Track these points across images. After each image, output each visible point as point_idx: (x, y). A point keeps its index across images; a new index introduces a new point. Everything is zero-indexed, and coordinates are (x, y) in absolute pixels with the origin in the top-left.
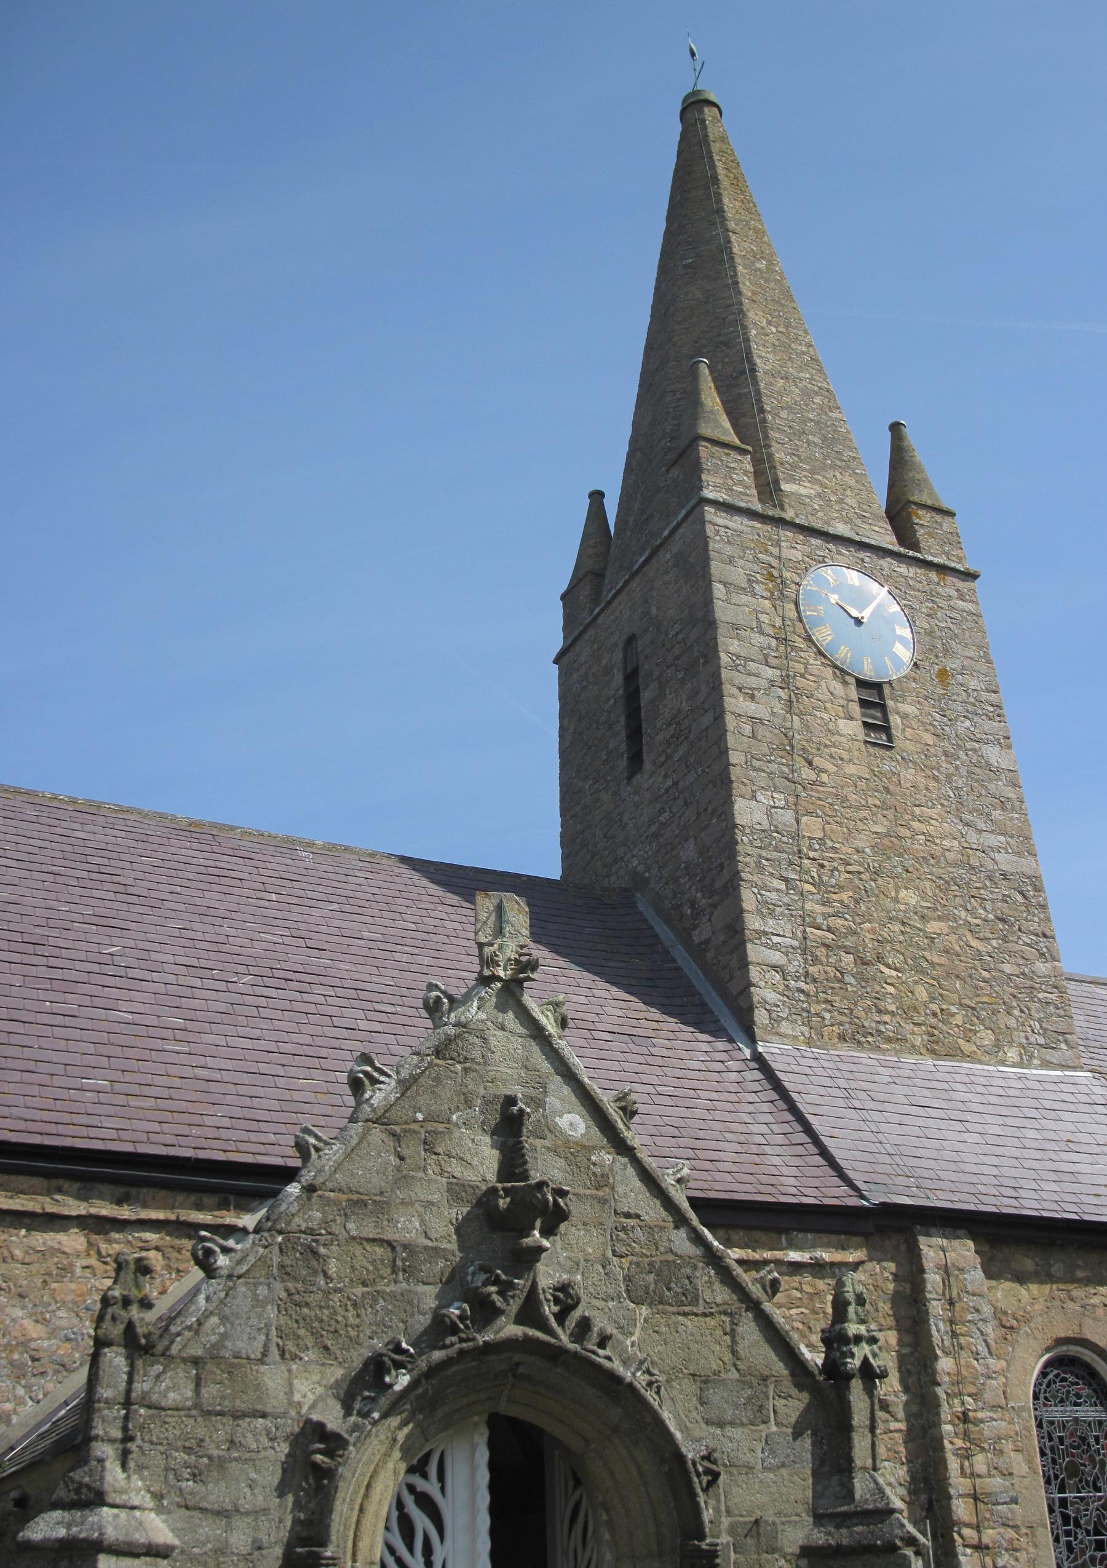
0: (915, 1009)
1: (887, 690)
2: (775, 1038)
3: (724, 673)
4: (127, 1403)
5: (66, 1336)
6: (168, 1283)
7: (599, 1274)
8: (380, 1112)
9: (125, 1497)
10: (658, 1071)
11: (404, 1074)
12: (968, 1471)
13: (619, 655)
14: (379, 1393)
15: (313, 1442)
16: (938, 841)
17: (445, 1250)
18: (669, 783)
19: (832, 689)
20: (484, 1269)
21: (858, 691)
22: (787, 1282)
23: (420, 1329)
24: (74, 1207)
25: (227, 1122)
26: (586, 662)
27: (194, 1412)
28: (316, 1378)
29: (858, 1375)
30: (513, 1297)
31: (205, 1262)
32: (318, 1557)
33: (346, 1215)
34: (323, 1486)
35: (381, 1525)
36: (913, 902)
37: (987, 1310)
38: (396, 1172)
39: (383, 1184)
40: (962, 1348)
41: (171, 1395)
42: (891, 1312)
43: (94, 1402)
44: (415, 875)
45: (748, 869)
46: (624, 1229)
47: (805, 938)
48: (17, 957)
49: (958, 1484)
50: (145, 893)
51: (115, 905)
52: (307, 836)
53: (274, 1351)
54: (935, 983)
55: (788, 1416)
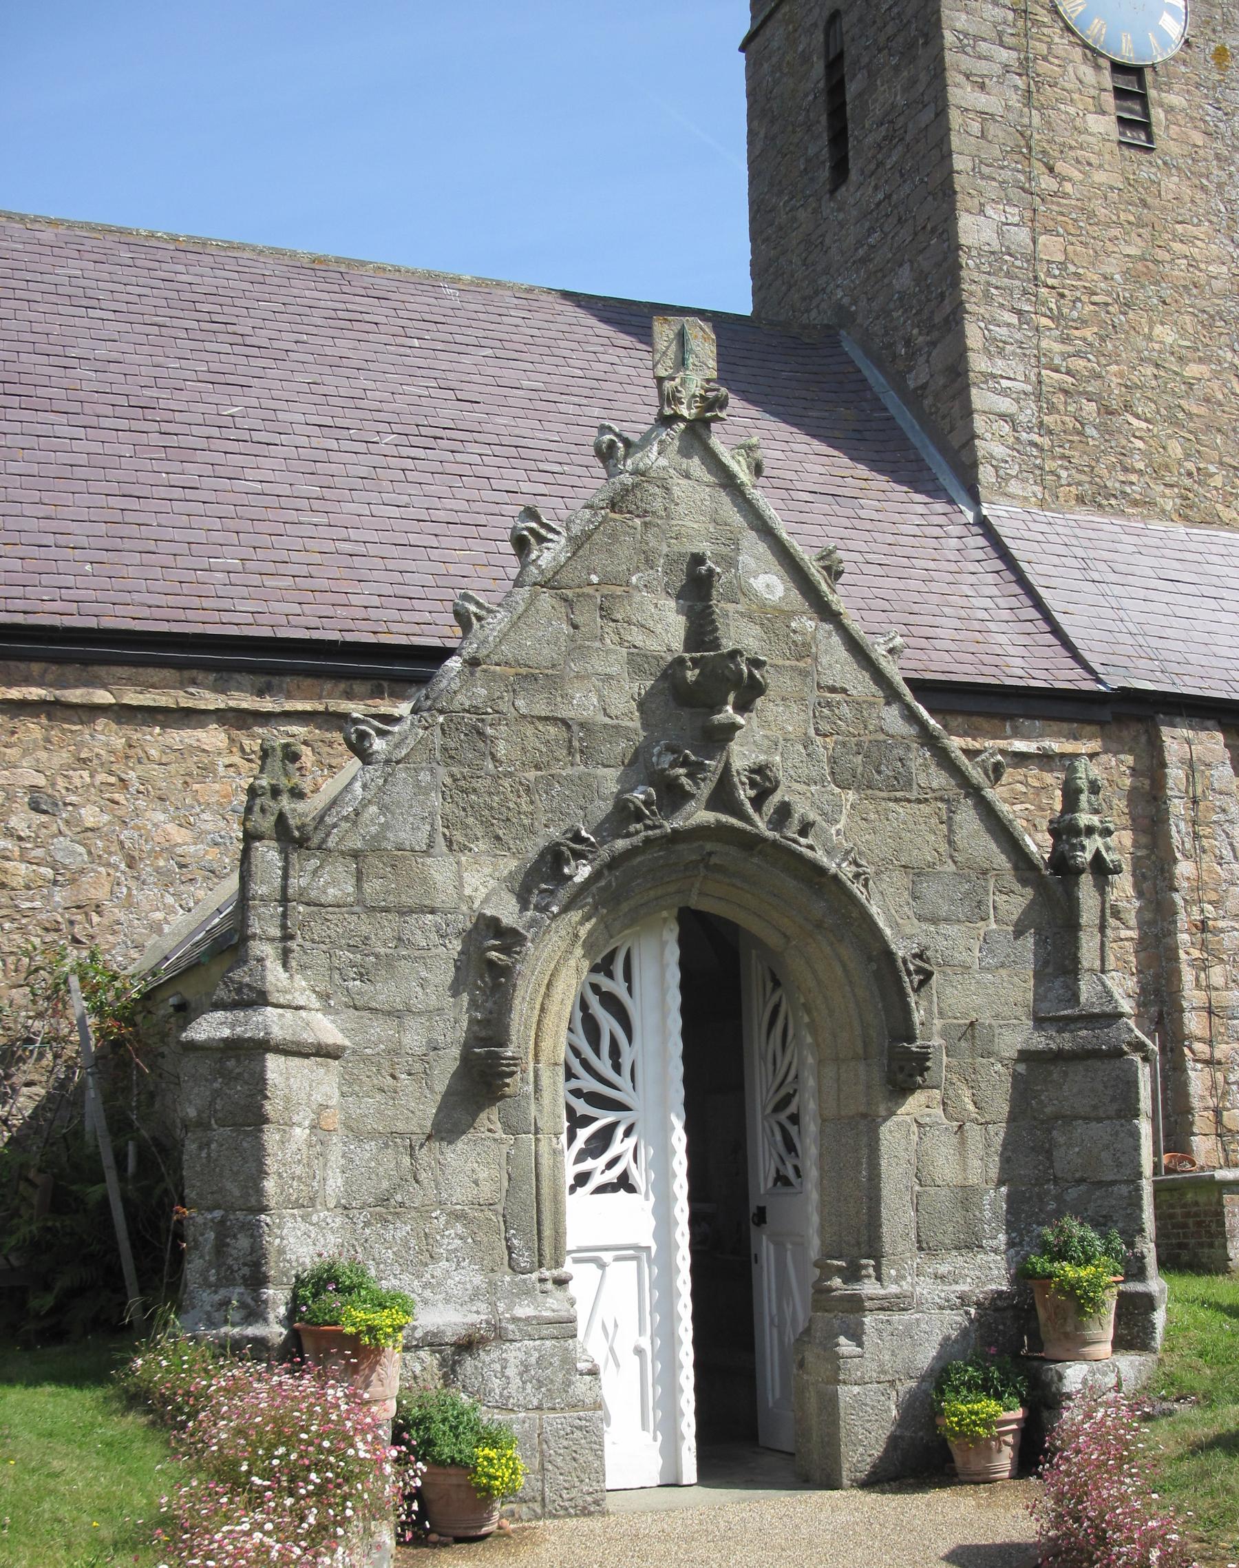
0: (1167, 467)
1: (1149, 76)
2: (1003, 500)
3: (949, 57)
4: (284, 900)
5: (213, 840)
6: (320, 780)
7: (800, 754)
8: (549, 575)
9: (289, 997)
10: (867, 536)
11: (576, 530)
12: (1204, 984)
13: (819, 37)
14: (557, 886)
15: (486, 938)
16: (1203, 266)
17: (627, 728)
18: (880, 196)
19: (1081, 76)
20: (670, 749)
21: (1113, 78)
22: (1011, 775)
23: (601, 815)
24: (210, 700)
25: (376, 601)
26: (779, 48)
27: (356, 909)
28: (487, 870)
29: (1089, 870)
30: (703, 780)
31: (360, 748)
32: (499, 1057)
33: (514, 691)
34: (501, 984)
35: (565, 1025)
36: (1169, 340)
38: (569, 643)
39: (555, 656)
40: (1204, 852)
41: (331, 891)
42: (1126, 811)
43: (248, 900)
44: (580, 313)
45: (973, 300)
46: (829, 705)
47: (1040, 382)
48: (124, 424)
49: (1191, 995)
50: (265, 343)
51: (233, 359)
52: (453, 271)
53: (440, 842)
54: (1192, 437)
55: (1010, 913)
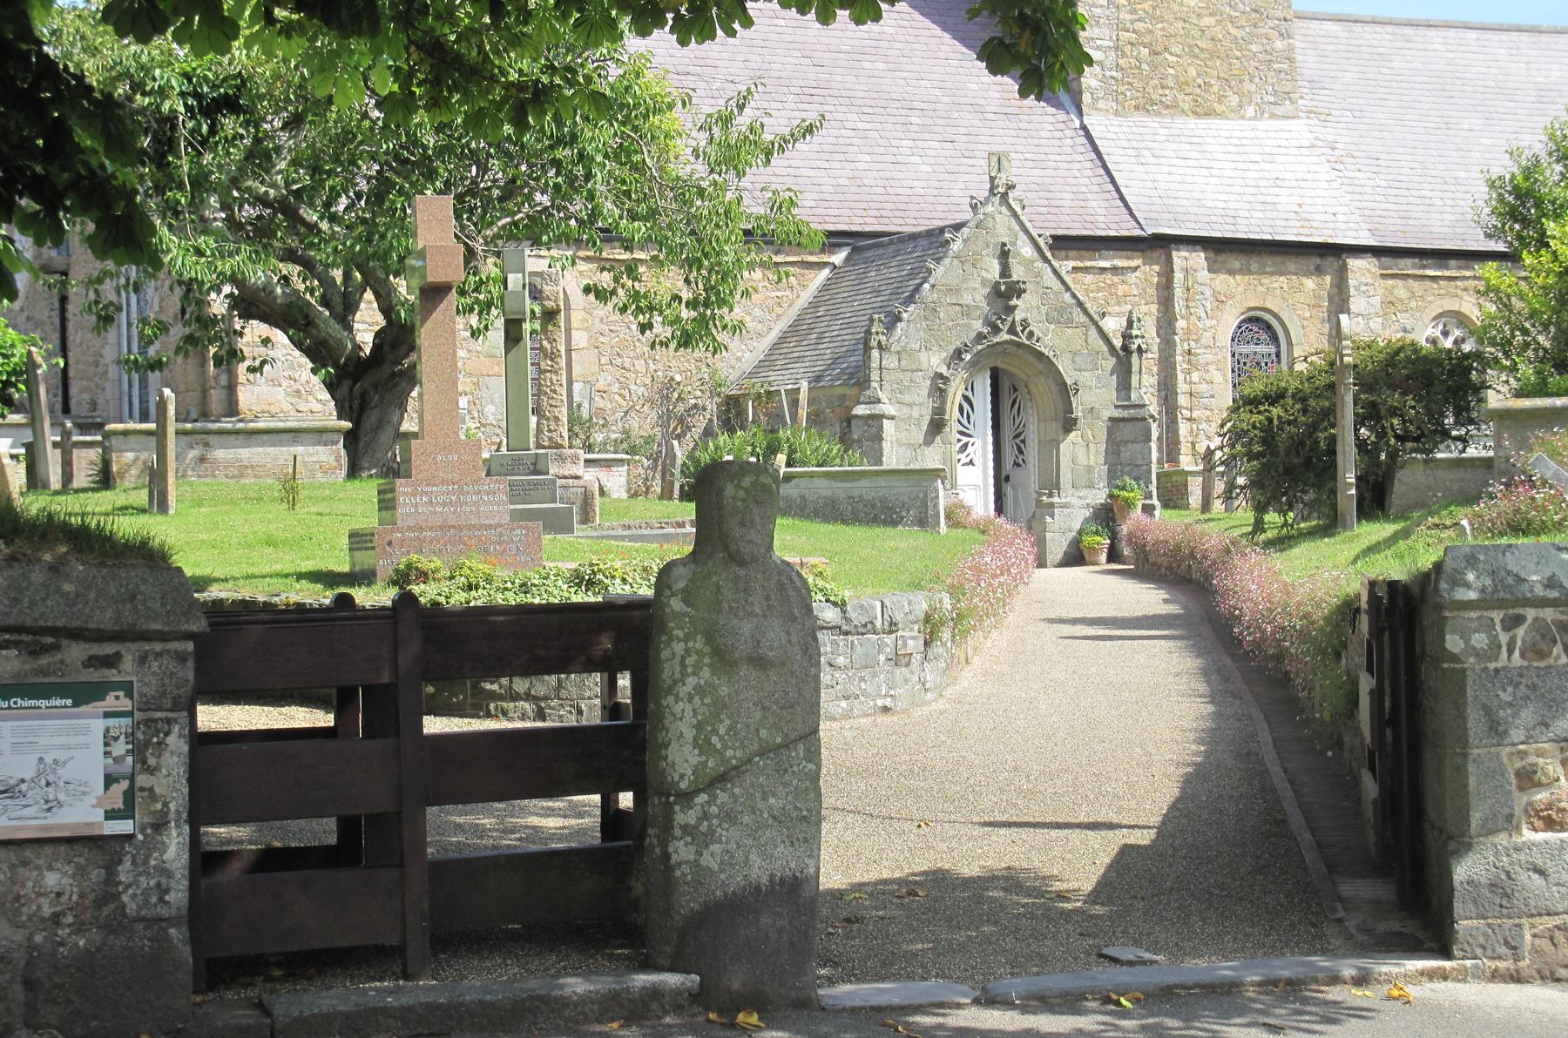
37: (1208, 293)
49: (1182, 387)
